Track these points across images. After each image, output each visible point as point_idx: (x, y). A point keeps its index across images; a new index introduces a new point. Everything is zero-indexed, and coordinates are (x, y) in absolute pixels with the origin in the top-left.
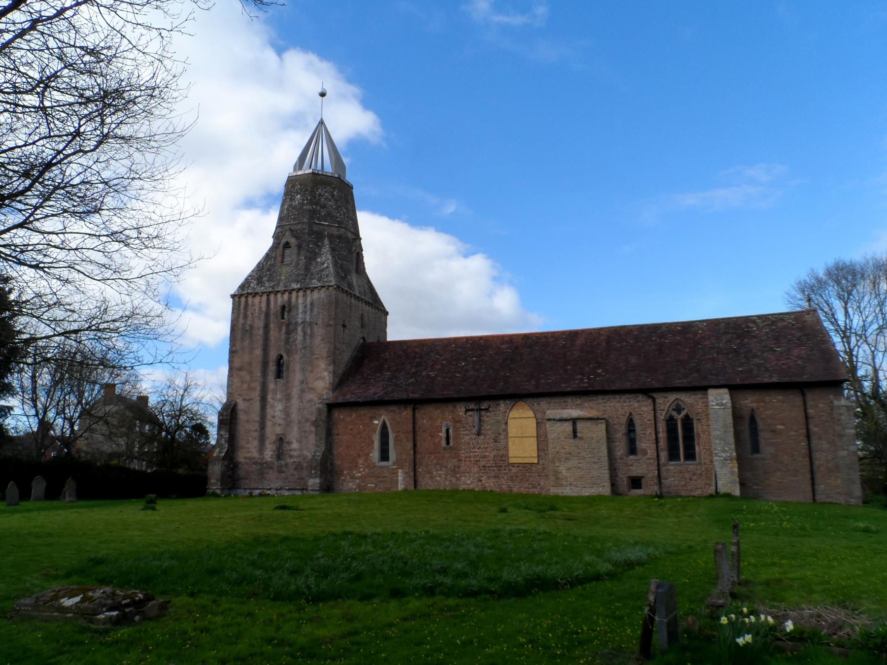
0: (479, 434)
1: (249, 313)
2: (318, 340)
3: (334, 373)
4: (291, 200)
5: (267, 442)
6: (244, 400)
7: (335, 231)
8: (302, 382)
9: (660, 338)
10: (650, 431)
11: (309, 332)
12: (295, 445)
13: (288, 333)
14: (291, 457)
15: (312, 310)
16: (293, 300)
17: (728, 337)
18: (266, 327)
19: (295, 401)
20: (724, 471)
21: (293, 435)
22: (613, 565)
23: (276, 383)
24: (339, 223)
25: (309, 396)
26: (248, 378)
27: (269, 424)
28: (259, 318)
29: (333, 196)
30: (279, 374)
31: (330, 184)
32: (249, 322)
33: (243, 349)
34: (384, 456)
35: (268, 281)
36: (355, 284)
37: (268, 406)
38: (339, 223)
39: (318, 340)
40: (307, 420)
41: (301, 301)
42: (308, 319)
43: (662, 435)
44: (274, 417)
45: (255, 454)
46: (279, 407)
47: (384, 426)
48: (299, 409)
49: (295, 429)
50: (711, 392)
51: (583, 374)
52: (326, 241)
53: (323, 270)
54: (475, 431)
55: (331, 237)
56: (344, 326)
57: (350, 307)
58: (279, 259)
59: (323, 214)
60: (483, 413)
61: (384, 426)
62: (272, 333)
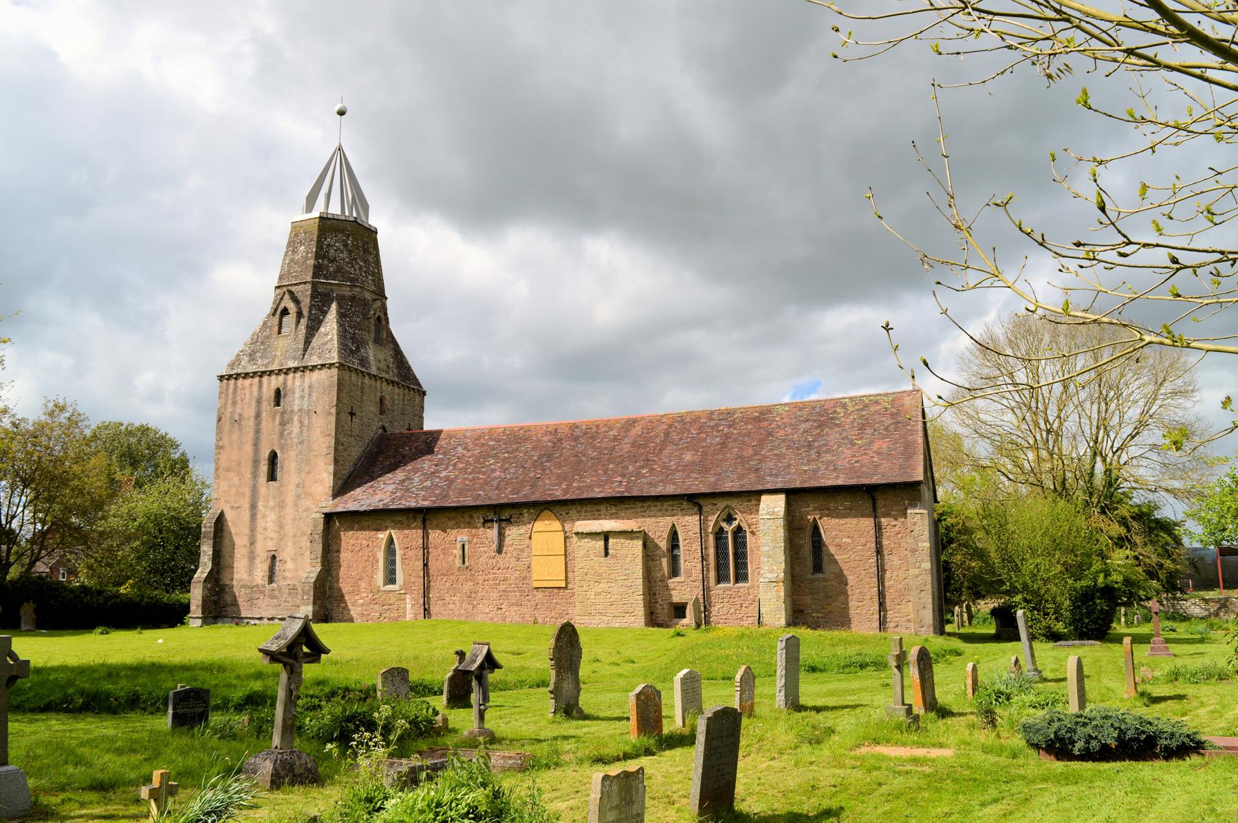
0: (499, 551)
1: (238, 398)
3: (335, 474)
4: (294, 252)
5: (258, 561)
6: (232, 508)
7: (347, 292)
8: (298, 486)
9: (729, 427)
10: (696, 546)
11: (306, 422)
12: (290, 565)
14: (285, 578)
15: (310, 395)
16: (290, 382)
17: (808, 425)
19: (289, 510)
20: (769, 595)
21: (286, 554)
22: (410, 723)
23: (268, 488)
24: (352, 280)
25: (307, 503)
26: (236, 481)
27: (259, 538)
28: (250, 404)
29: (346, 245)
30: (272, 477)
31: (343, 231)
32: (238, 411)
33: (231, 443)
34: (391, 578)
35: (261, 357)
36: (371, 358)
37: (259, 516)
38: (352, 280)
40: (303, 534)
41: (297, 383)
42: (305, 407)
43: (711, 551)
44: (265, 529)
45: (245, 576)
46: (272, 516)
47: (391, 541)
48: (294, 519)
49: (290, 544)
50: (764, 498)
51: (623, 476)
52: (334, 306)
53: (326, 344)
54: (494, 547)
55: (341, 300)
56: (352, 414)
57: (362, 388)
58: (276, 328)
59: (331, 269)
60: (504, 525)
61: (391, 541)
62: (264, 423)
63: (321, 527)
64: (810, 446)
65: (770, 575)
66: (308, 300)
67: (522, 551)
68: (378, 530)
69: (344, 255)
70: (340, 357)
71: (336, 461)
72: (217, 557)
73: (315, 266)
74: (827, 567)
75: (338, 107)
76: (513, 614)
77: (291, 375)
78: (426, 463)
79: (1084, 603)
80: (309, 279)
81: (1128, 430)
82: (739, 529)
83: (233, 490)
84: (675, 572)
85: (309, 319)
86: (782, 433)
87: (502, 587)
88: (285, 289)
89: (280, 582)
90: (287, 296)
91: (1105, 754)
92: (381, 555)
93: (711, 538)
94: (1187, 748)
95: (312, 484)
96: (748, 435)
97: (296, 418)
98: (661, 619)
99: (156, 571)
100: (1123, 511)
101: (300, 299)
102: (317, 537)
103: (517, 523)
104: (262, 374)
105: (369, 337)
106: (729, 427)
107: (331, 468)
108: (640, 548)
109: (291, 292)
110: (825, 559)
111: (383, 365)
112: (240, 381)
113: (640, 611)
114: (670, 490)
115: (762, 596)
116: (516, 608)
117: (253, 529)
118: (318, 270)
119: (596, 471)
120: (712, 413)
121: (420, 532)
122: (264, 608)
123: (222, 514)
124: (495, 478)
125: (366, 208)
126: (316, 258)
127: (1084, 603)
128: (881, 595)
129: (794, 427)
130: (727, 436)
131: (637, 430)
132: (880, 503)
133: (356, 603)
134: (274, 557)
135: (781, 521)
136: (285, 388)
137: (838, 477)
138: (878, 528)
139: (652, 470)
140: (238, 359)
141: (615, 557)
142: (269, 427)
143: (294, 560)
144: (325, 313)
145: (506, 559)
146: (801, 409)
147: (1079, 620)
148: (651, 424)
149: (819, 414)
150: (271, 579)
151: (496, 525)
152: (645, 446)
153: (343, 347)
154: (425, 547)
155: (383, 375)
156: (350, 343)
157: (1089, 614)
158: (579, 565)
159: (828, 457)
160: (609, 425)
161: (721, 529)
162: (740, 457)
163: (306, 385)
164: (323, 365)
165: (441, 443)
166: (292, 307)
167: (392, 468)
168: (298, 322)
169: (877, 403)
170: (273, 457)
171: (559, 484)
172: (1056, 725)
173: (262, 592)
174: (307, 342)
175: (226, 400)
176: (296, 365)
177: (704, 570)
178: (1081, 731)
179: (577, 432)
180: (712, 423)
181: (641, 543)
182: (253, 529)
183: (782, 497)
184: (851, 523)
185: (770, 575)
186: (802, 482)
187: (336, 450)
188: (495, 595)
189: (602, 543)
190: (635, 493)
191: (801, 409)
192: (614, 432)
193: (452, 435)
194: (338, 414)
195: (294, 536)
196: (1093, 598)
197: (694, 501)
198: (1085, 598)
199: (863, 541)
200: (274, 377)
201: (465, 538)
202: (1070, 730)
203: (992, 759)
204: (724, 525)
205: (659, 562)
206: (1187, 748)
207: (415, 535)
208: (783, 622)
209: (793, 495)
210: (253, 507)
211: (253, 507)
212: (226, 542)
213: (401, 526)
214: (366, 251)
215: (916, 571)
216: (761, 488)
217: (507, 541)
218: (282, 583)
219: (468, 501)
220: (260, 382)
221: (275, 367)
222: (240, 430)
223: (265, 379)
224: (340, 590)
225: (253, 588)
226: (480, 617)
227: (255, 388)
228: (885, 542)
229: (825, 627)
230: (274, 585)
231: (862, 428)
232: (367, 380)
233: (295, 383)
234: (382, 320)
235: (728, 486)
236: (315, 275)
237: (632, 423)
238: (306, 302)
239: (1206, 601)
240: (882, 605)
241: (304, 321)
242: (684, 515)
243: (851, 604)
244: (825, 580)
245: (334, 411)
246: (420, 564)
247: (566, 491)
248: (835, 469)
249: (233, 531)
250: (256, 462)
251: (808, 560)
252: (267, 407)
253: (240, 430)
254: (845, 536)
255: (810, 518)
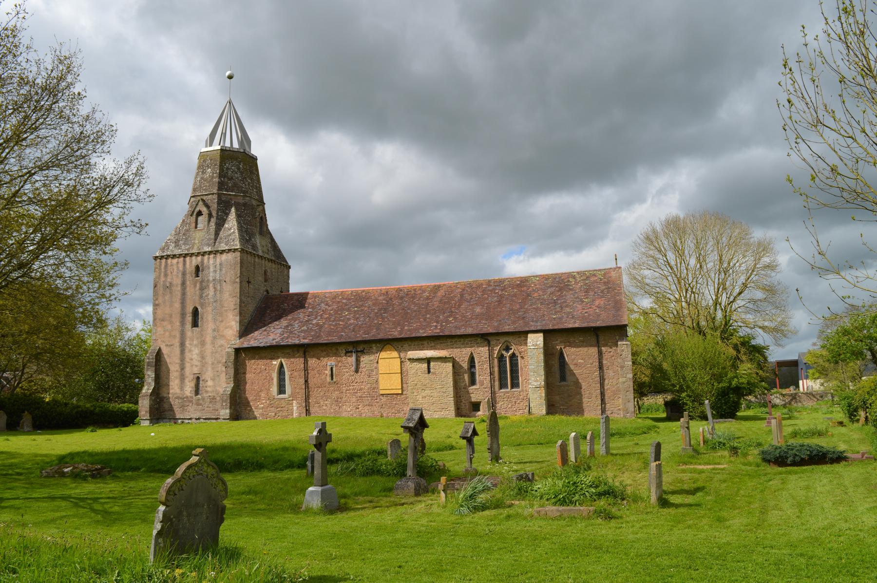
0: (357, 371)
1: (169, 272)
2: (226, 295)
3: (240, 322)
4: (203, 173)
5: (187, 381)
6: (167, 345)
7: (241, 201)
8: (214, 330)
9: (502, 290)
10: (486, 366)
11: (219, 288)
12: (210, 383)
13: (202, 289)
14: (207, 392)
15: (221, 270)
17: (553, 289)
18: (183, 283)
19: (209, 347)
21: (208, 375)
23: (193, 332)
26: (169, 327)
27: (188, 365)
29: (239, 169)
30: (195, 324)
31: (236, 159)
32: (169, 280)
34: (281, 390)
36: (259, 245)
37: (187, 351)
39: (226, 295)
40: (219, 362)
41: (211, 262)
42: (218, 278)
43: (496, 369)
44: (192, 359)
45: (178, 391)
46: (196, 351)
47: (281, 366)
48: (212, 353)
49: (210, 369)
50: (529, 335)
51: (437, 322)
52: (233, 210)
53: (230, 235)
54: (353, 368)
55: (238, 206)
56: (249, 282)
57: (254, 265)
58: (194, 225)
60: (359, 354)
61: (281, 366)
62: (188, 289)
63: (233, 357)
64: (555, 302)
65: (535, 384)
66: (216, 206)
67: (372, 371)
68: (272, 359)
69: (238, 175)
70: (241, 245)
71: (241, 314)
72: (157, 379)
73: (219, 183)
74: (569, 378)
75: (228, 73)
76: (366, 411)
77: (206, 256)
78: (301, 314)
79: (723, 397)
80: (215, 191)
81: (737, 290)
82: (514, 355)
83: (167, 334)
84: (473, 382)
85: (217, 218)
86: (536, 294)
87: (359, 394)
88: (199, 198)
89: (203, 394)
90: (201, 203)
91: (802, 463)
92: (275, 376)
93: (496, 361)
94: (838, 458)
95: (225, 329)
96: (515, 295)
97: (211, 285)
98: (464, 413)
99: (99, 389)
100: (734, 340)
101: (210, 205)
102: (230, 364)
103: (369, 353)
104: (185, 256)
105: (256, 230)
106: (502, 290)
107: (238, 318)
108: (451, 368)
109: (203, 200)
110: (568, 373)
111: (265, 249)
112: (169, 260)
113: (452, 408)
114: (470, 331)
115: (531, 396)
116: (368, 408)
117: (182, 359)
118: (221, 185)
119: (419, 319)
120: (490, 281)
121: (302, 360)
122: (192, 412)
123: (160, 349)
124: (351, 324)
125: (249, 142)
126: (220, 177)
127: (723, 397)
128: (602, 394)
129: (544, 291)
130: (501, 296)
131: (441, 293)
132: (601, 338)
133: (258, 407)
134: (198, 378)
135: (542, 350)
136: (203, 265)
137: (575, 322)
138: (600, 353)
139: (455, 318)
140: (167, 245)
141: (434, 373)
142: (192, 291)
143: (213, 380)
144: (227, 215)
145: (362, 376)
146: (547, 279)
147: (720, 407)
148: (451, 289)
149: (558, 282)
150: (197, 392)
151: (354, 355)
152: (449, 303)
153: (242, 239)
154: (306, 369)
155: (266, 256)
156: (246, 234)
157: (726, 403)
158: (411, 380)
159: (568, 310)
160: (422, 289)
161: (502, 355)
162: (512, 310)
163: (218, 263)
164: (230, 250)
165: (309, 301)
166: (204, 210)
167: (278, 318)
168: (209, 221)
169: (595, 275)
170: (195, 312)
171: (395, 328)
172: (778, 451)
173: (191, 401)
174: (217, 234)
175: (160, 273)
176: (210, 249)
177: (492, 380)
178: (790, 452)
179: (402, 294)
180: (490, 288)
181: (451, 364)
182: (182, 359)
183: (542, 334)
184: (583, 350)
185: (535, 384)
186: (553, 325)
187: (240, 306)
188: (354, 399)
189: (426, 365)
190: (447, 333)
191: (547, 279)
192: (427, 294)
193: (315, 296)
194: (241, 282)
195: (213, 364)
196: (728, 394)
197: (485, 338)
198: (724, 394)
199: (591, 361)
200: (194, 258)
201: (333, 363)
202: (785, 452)
203: (749, 468)
204: (504, 352)
205: (464, 376)
206: (838, 458)
207: (299, 362)
208: (544, 412)
209: (548, 334)
210: (182, 345)
211: (182, 345)
212: (163, 368)
213: (288, 356)
214: (251, 172)
215: (624, 380)
216: (527, 329)
217: (362, 365)
218: (205, 395)
219: (335, 339)
220: (184, 261)
221: (195, 251)
222: (171, 293)
223: (188, 259)
224: (247, 398)
225: (185, 401)
226: (344, 414)
227: (181, 265)
228: (604, 362)
229: (563, 413)
230: (199, 396)
231: (587, 291)
232: (257, 260)
233: (210, 261)
234: (263, 220)
235: (507, 329)
236: (220, 189)
237: (437, 288)
238: (214, 206)
239: (783, 395)
240: (603, 400)
241: (213, 220)
242: (478, 347)
243: (584, 400)
244: (568, 386)
245: (238, 280)
246: (302, 381)
247: (401, 332)
248: (573, 317)
249: (168, 361)
250: (183, 315)
251: (557, 372)
252: (189, 278)
253: (171, 293)
254: (580, 359)
255: (558, 347)
